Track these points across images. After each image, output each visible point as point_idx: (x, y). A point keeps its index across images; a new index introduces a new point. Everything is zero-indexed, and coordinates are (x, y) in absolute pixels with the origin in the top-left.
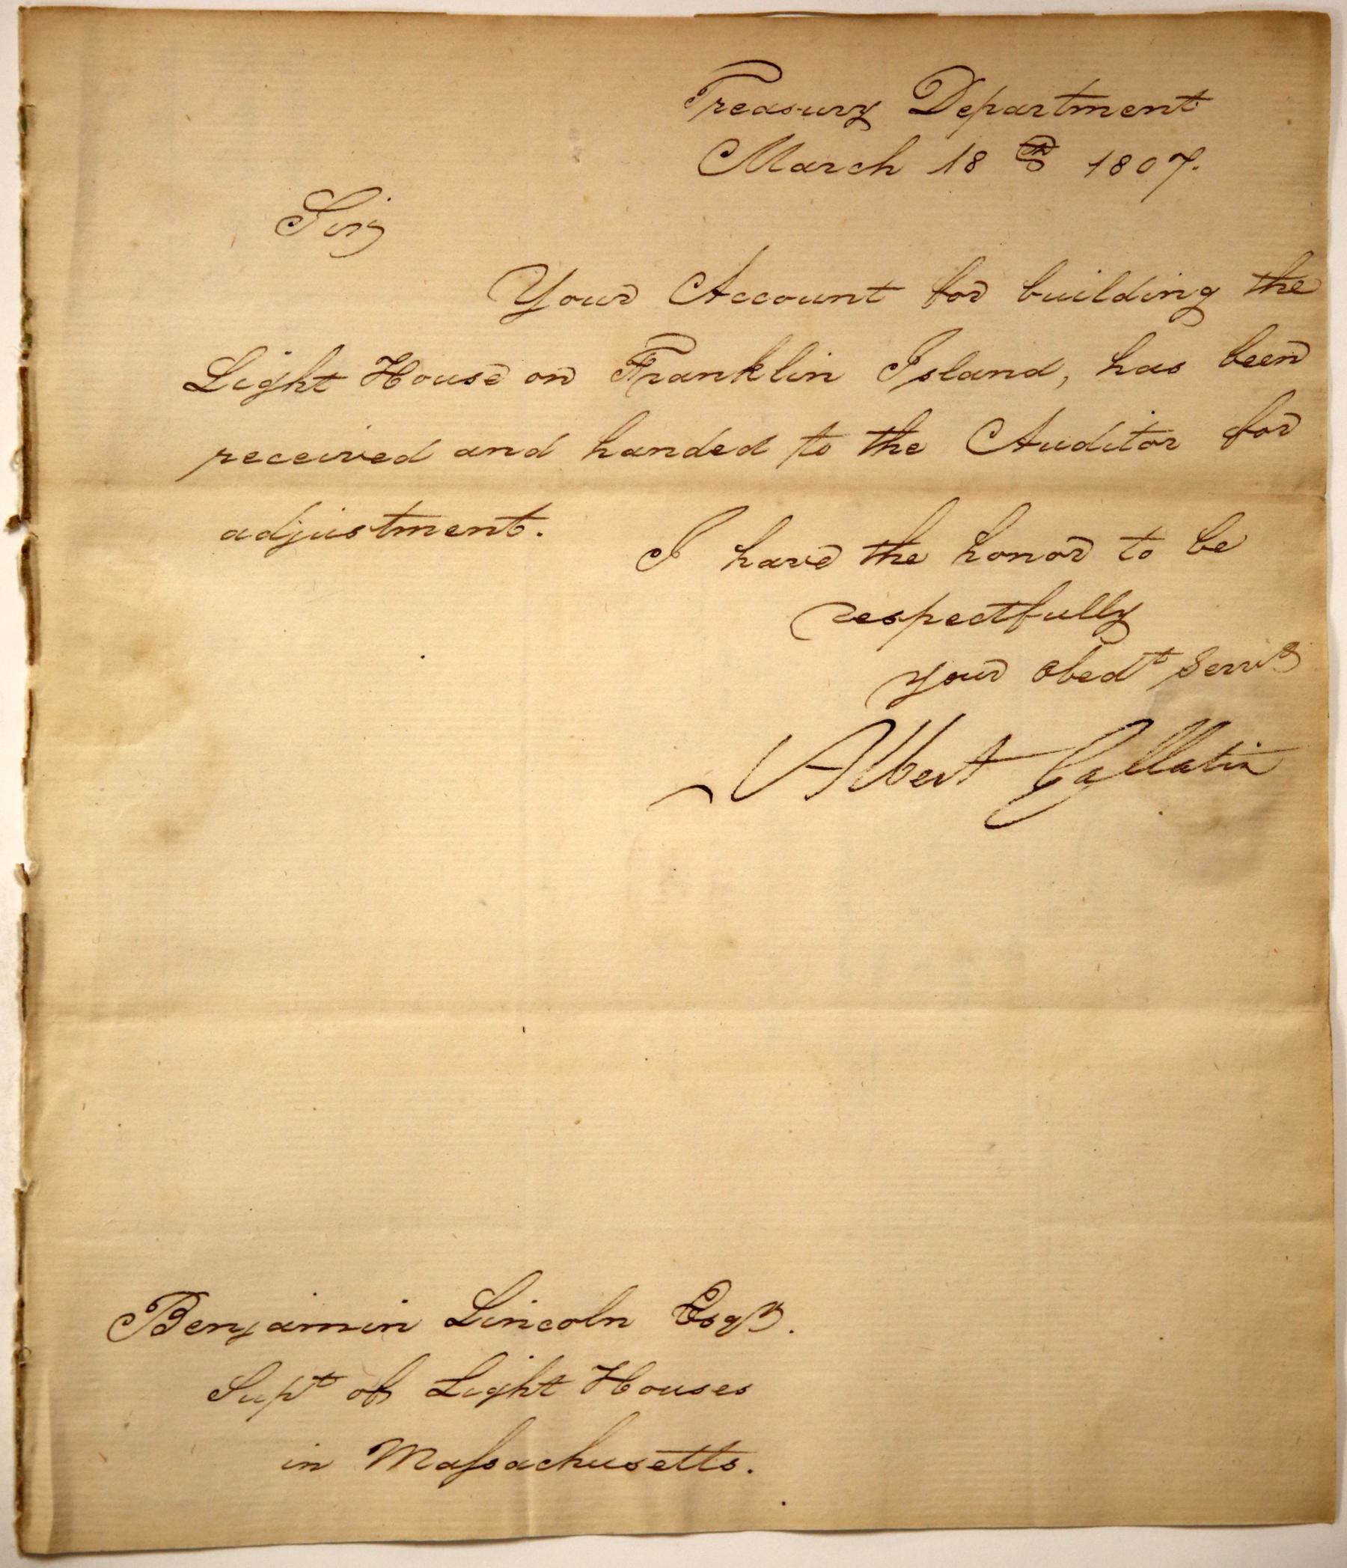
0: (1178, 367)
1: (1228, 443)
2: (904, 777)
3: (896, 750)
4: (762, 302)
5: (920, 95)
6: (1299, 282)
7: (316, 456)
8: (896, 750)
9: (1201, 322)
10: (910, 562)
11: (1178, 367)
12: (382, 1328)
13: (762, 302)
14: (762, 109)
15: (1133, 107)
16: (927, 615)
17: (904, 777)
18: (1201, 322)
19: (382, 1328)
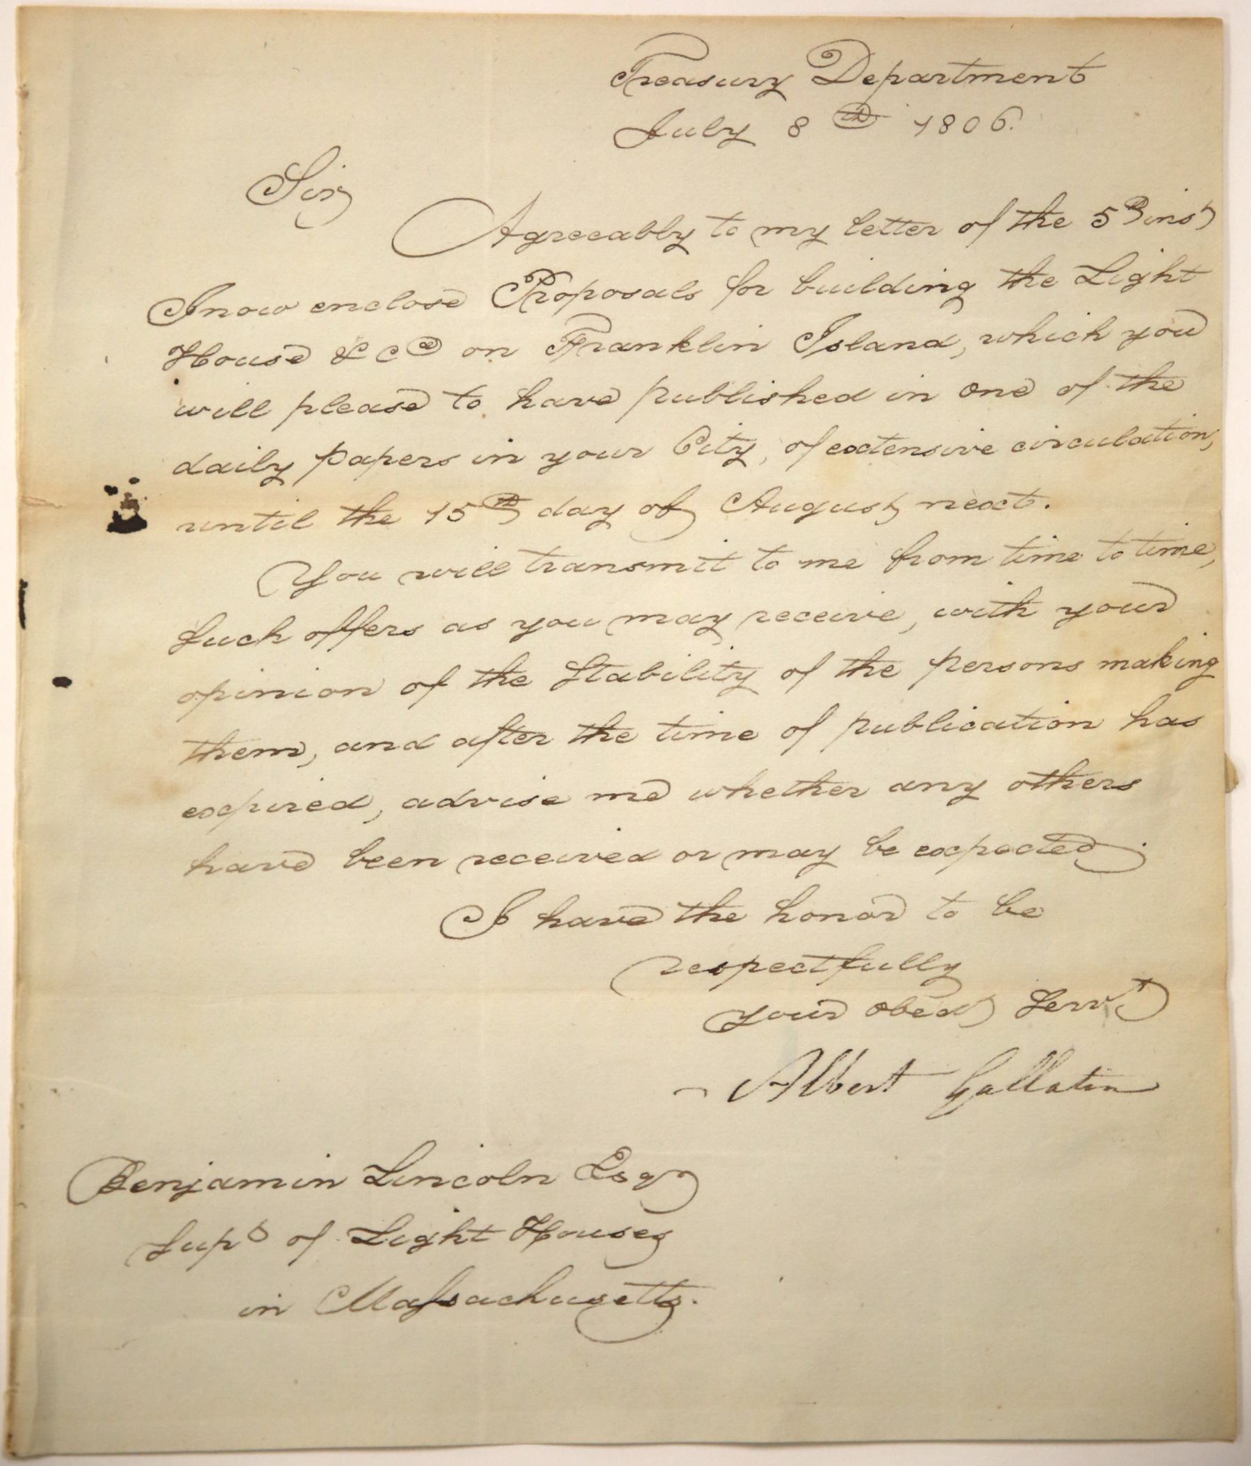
0: (1190, 217)
1: (800, 289)
2: (737, 1089)
3: (713, 1017)
4: (461, 1187)
5: (579, 1176)
6: (476, 401)
7: (954, 285)
8: (713, 1017)
9: (618, 132)
10: (729, 920)
11: (1190, 217)
12: (641, 618)
13: (461, 1187)
14: (404, 1303)
15: (1024, 75)
16: (782, 914)
17: (737, 1089)
18: (618, 132)
19: (641, 618)
